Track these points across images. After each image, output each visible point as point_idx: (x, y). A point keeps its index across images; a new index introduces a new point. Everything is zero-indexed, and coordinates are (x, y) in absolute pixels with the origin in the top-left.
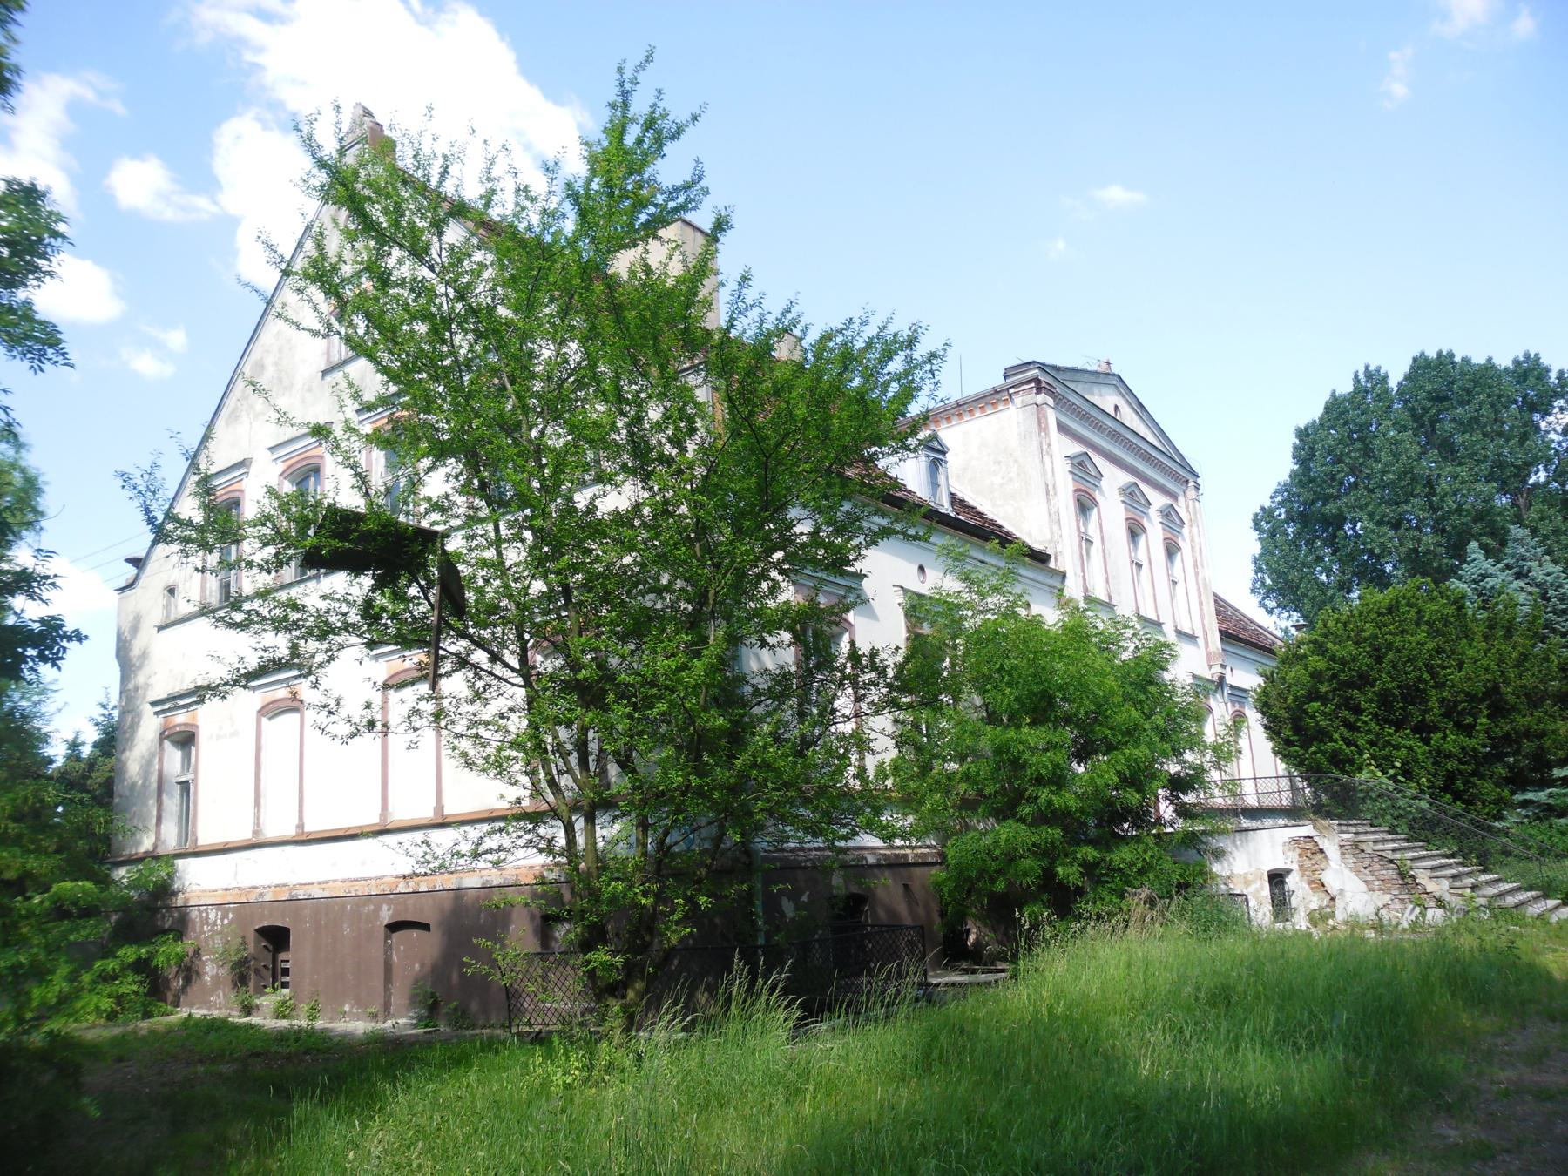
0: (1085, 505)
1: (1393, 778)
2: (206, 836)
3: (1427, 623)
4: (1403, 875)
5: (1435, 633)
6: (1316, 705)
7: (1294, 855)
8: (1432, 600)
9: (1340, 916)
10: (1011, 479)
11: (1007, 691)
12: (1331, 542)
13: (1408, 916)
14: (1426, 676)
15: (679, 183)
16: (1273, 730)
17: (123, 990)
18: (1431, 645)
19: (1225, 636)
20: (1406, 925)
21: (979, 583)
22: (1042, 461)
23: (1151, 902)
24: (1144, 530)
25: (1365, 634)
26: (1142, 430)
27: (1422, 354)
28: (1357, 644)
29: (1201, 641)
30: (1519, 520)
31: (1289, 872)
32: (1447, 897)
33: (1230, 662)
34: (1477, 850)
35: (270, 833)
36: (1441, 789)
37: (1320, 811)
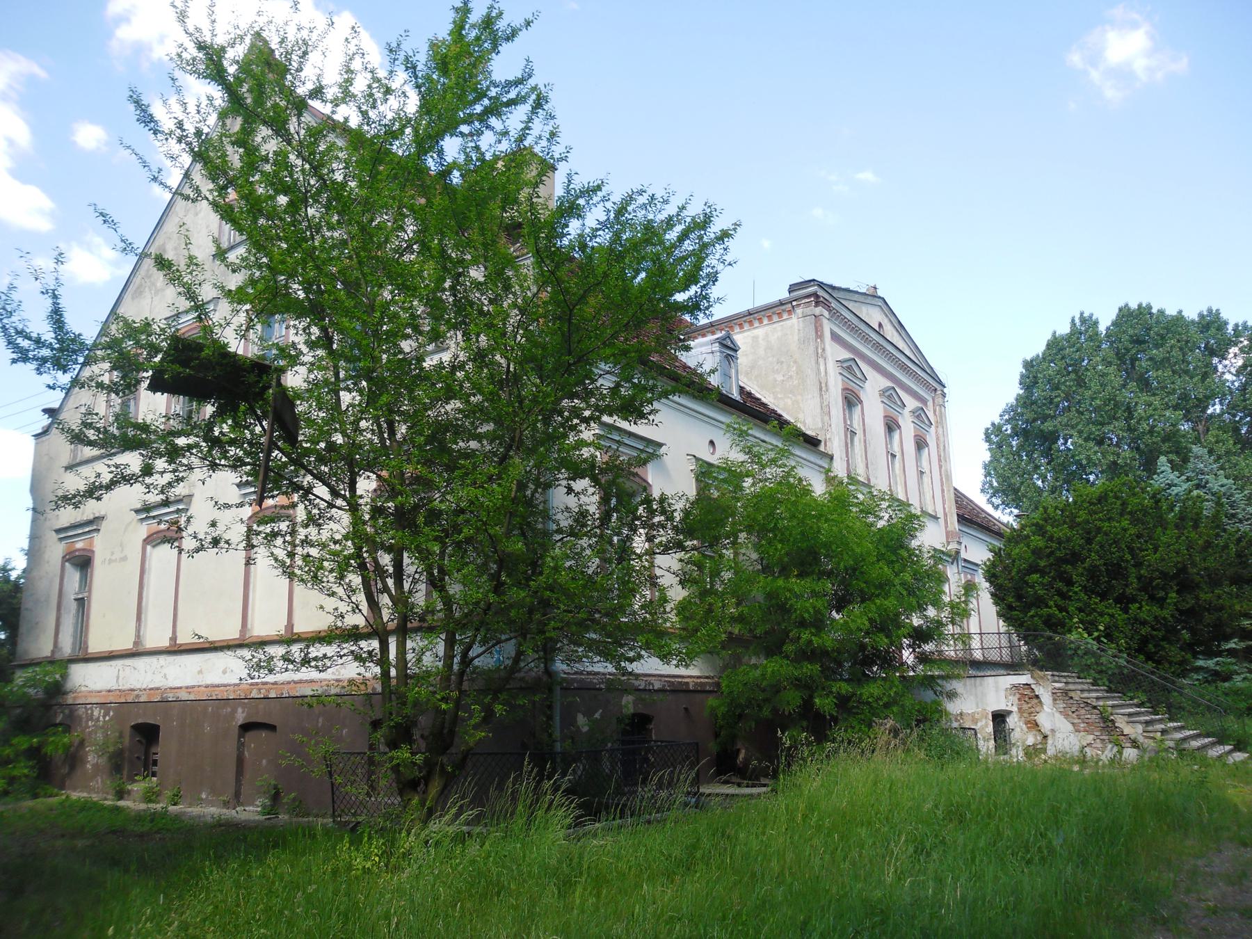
0: (851, 400)
1: (1098, 639)
2: (96, 645)
3: (1131, 513)
4: (1105, 719)
5: (1135, 521)
6: (1035, 576)
8: (1134, 495)
9: (1051, 751)
11: (779, 546)
12: (1047, 453)
13: (1109, 753)
14: (1128, 557)
15: (511, 78)
16: (998, 597)
17: (16, 773)
18: (1133, 531)
19: (962, 519)
21: (758, 456)
22: (817, 362)
23: (895, 732)
24: (899, 427)
25: (1078, 520)
26: (901, 345)
27: (1127, 305)
28: (1071, 528)
29: (942, 521)
30: (1197, 441)
31: (1010, 712)
32: (1141, 739)
33: (965, 541)
34: (1160, 700)
35: (150, 644)
36: (1136, 651)
37: (1036, 665)
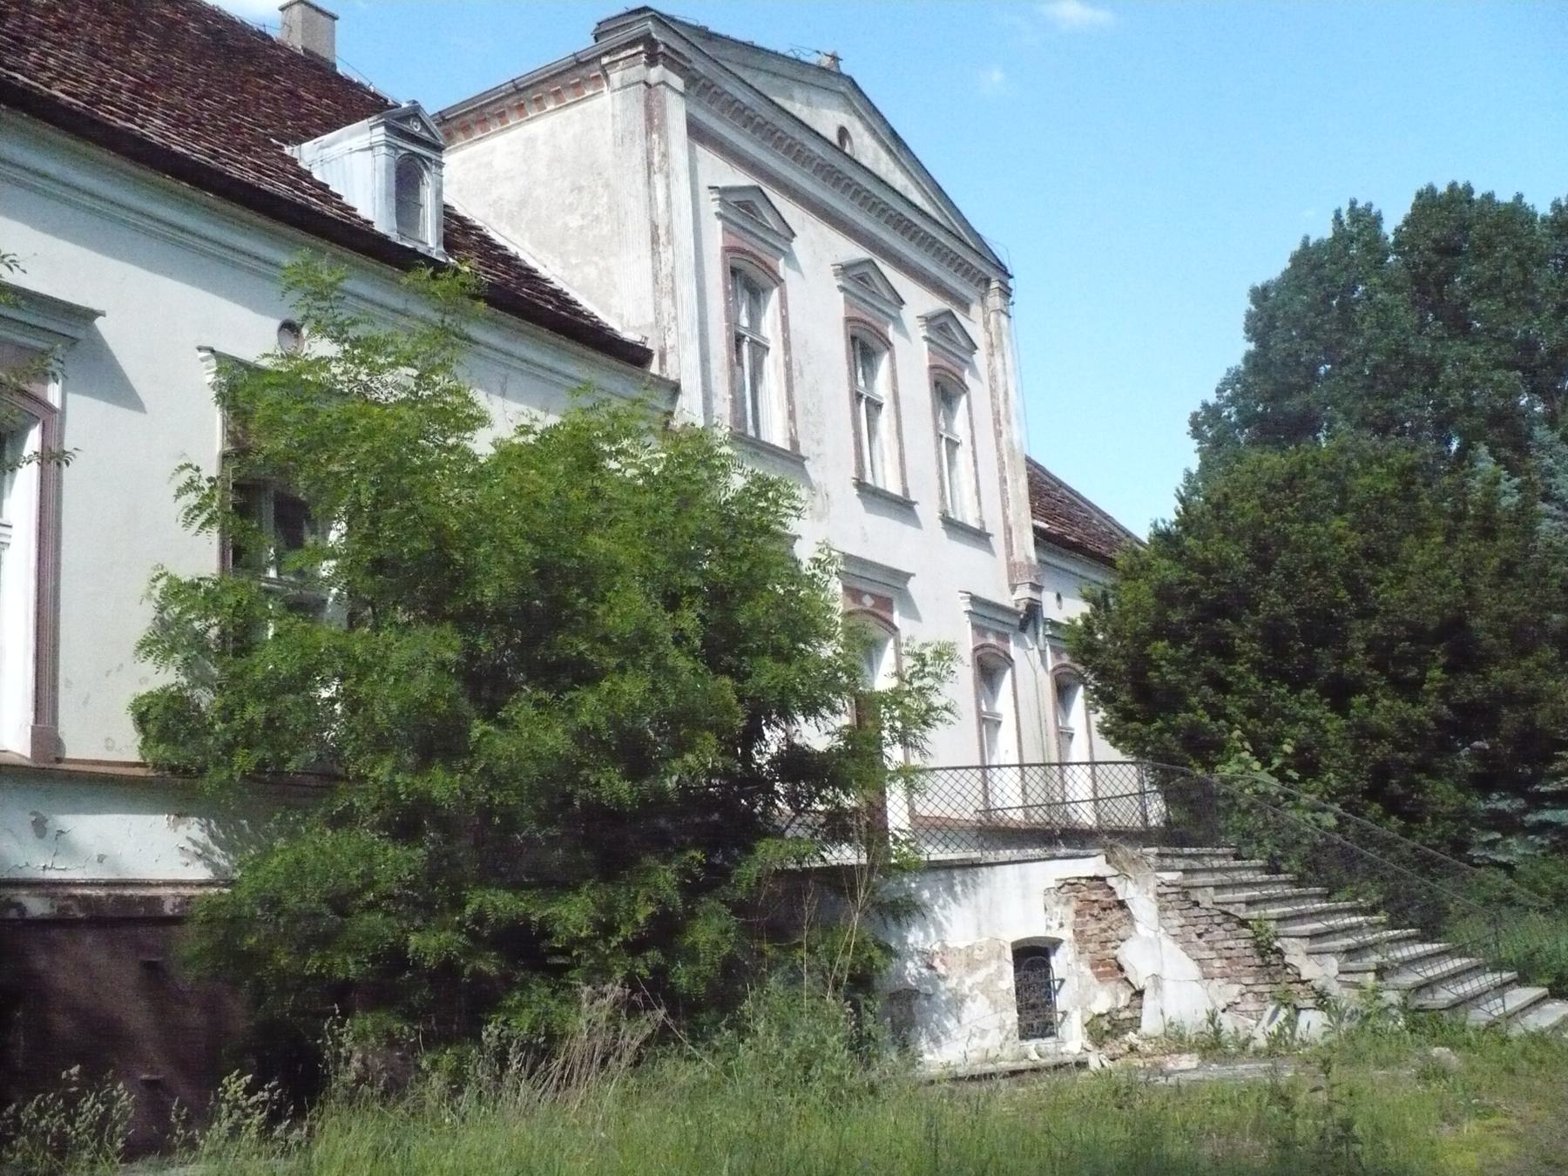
1: (1279, 773)
3: (1358, 508)
5: (1364, 524)
6: (1161, 645)
7: (1067, 913)
9: (1151, 1023)
10: (597, 218)
18: (1355, 540)
20: (1262, 1042)
24: (888, 345)
26: (899, 180)
29: (998, 541)
31: (1056, 943)
32: (1335, 989)
